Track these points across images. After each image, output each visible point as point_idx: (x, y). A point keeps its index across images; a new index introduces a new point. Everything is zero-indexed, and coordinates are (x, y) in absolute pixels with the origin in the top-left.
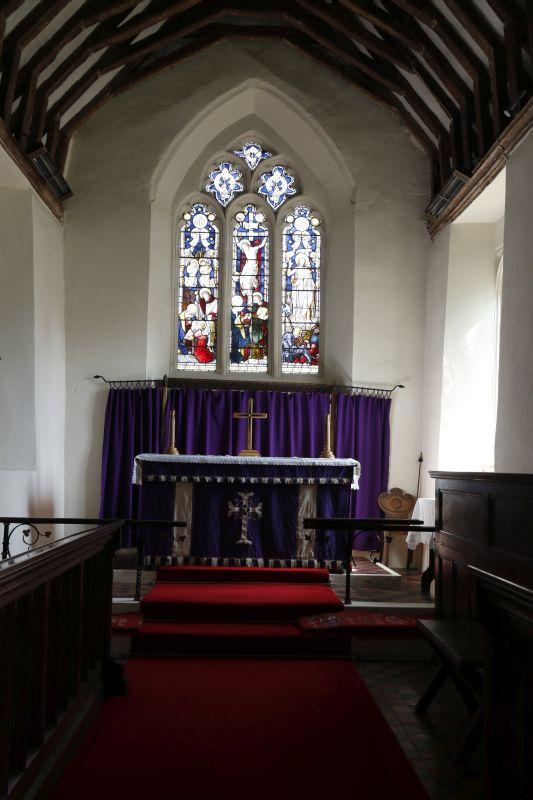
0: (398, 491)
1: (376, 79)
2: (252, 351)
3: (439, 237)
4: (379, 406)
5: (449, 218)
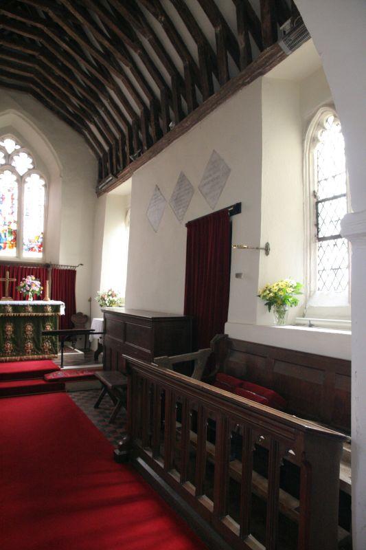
0: (80, 314)
1: (76, 121)
2: (7, 245)
3: (102, 197)
4: (70, 275)
5: (106, 191)
